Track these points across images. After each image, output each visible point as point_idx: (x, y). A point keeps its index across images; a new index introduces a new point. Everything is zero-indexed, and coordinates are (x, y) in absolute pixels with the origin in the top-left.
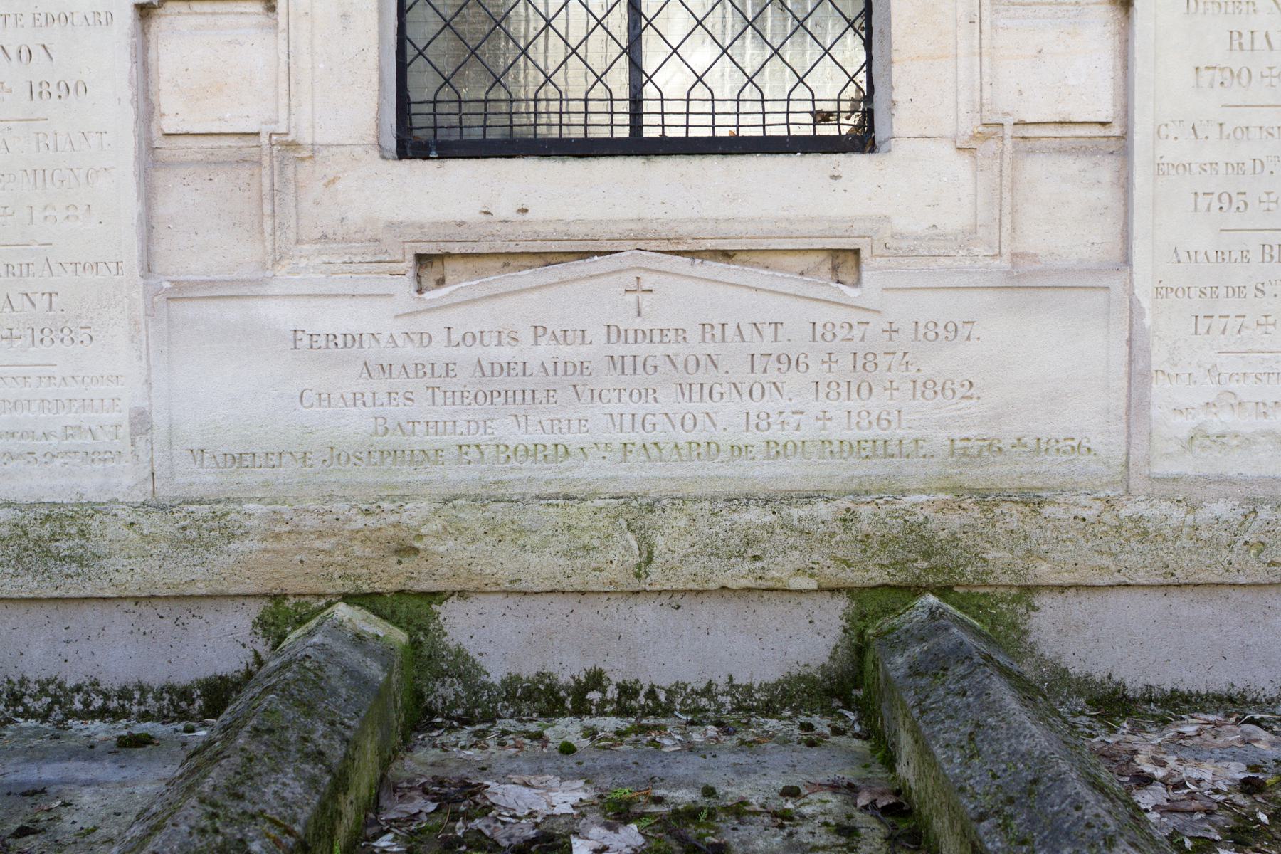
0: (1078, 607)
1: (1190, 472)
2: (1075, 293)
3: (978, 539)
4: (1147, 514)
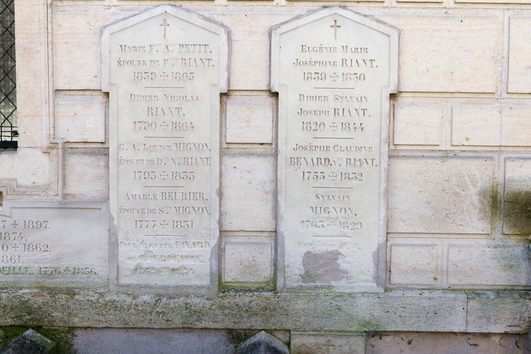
0: (92, 336)
1: (135, 283)
2: (87, 211)
3: (50, 308)
4: (117, 299)
